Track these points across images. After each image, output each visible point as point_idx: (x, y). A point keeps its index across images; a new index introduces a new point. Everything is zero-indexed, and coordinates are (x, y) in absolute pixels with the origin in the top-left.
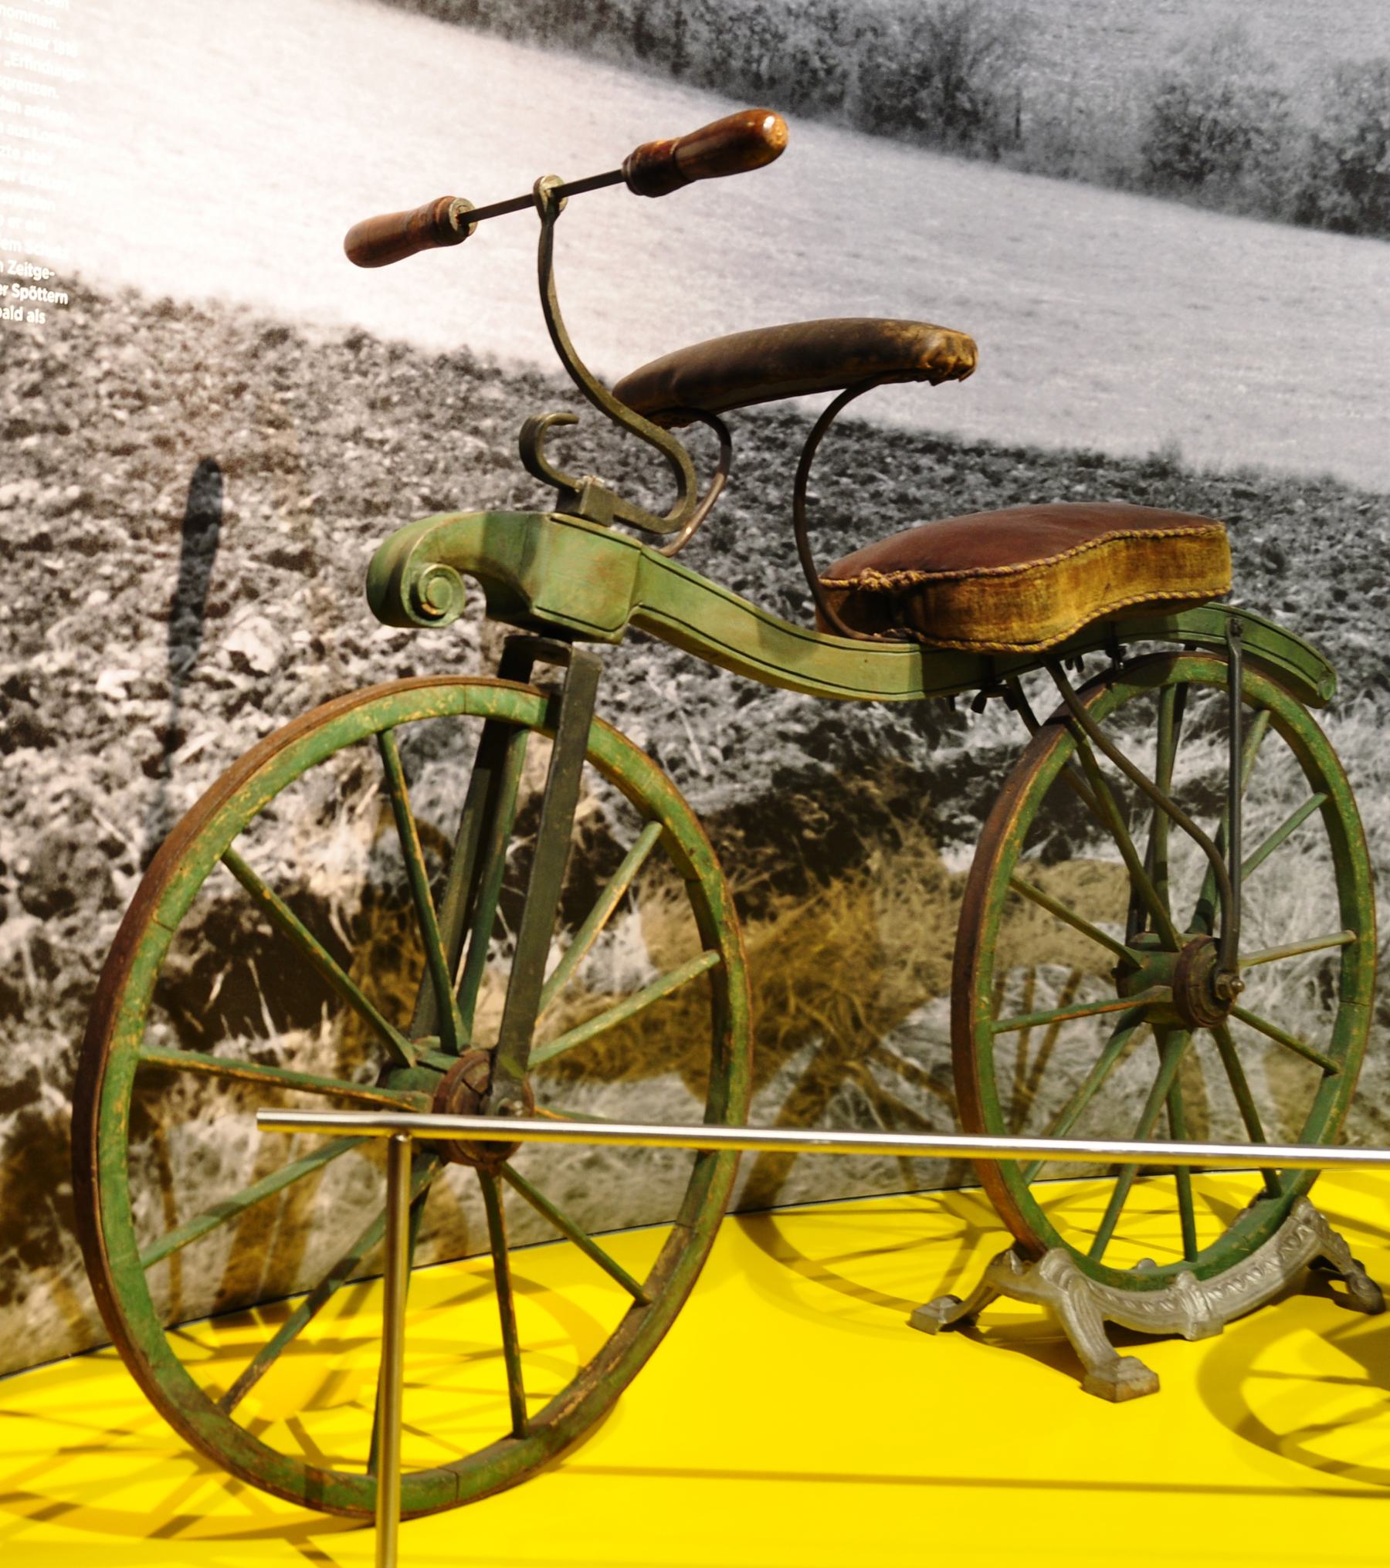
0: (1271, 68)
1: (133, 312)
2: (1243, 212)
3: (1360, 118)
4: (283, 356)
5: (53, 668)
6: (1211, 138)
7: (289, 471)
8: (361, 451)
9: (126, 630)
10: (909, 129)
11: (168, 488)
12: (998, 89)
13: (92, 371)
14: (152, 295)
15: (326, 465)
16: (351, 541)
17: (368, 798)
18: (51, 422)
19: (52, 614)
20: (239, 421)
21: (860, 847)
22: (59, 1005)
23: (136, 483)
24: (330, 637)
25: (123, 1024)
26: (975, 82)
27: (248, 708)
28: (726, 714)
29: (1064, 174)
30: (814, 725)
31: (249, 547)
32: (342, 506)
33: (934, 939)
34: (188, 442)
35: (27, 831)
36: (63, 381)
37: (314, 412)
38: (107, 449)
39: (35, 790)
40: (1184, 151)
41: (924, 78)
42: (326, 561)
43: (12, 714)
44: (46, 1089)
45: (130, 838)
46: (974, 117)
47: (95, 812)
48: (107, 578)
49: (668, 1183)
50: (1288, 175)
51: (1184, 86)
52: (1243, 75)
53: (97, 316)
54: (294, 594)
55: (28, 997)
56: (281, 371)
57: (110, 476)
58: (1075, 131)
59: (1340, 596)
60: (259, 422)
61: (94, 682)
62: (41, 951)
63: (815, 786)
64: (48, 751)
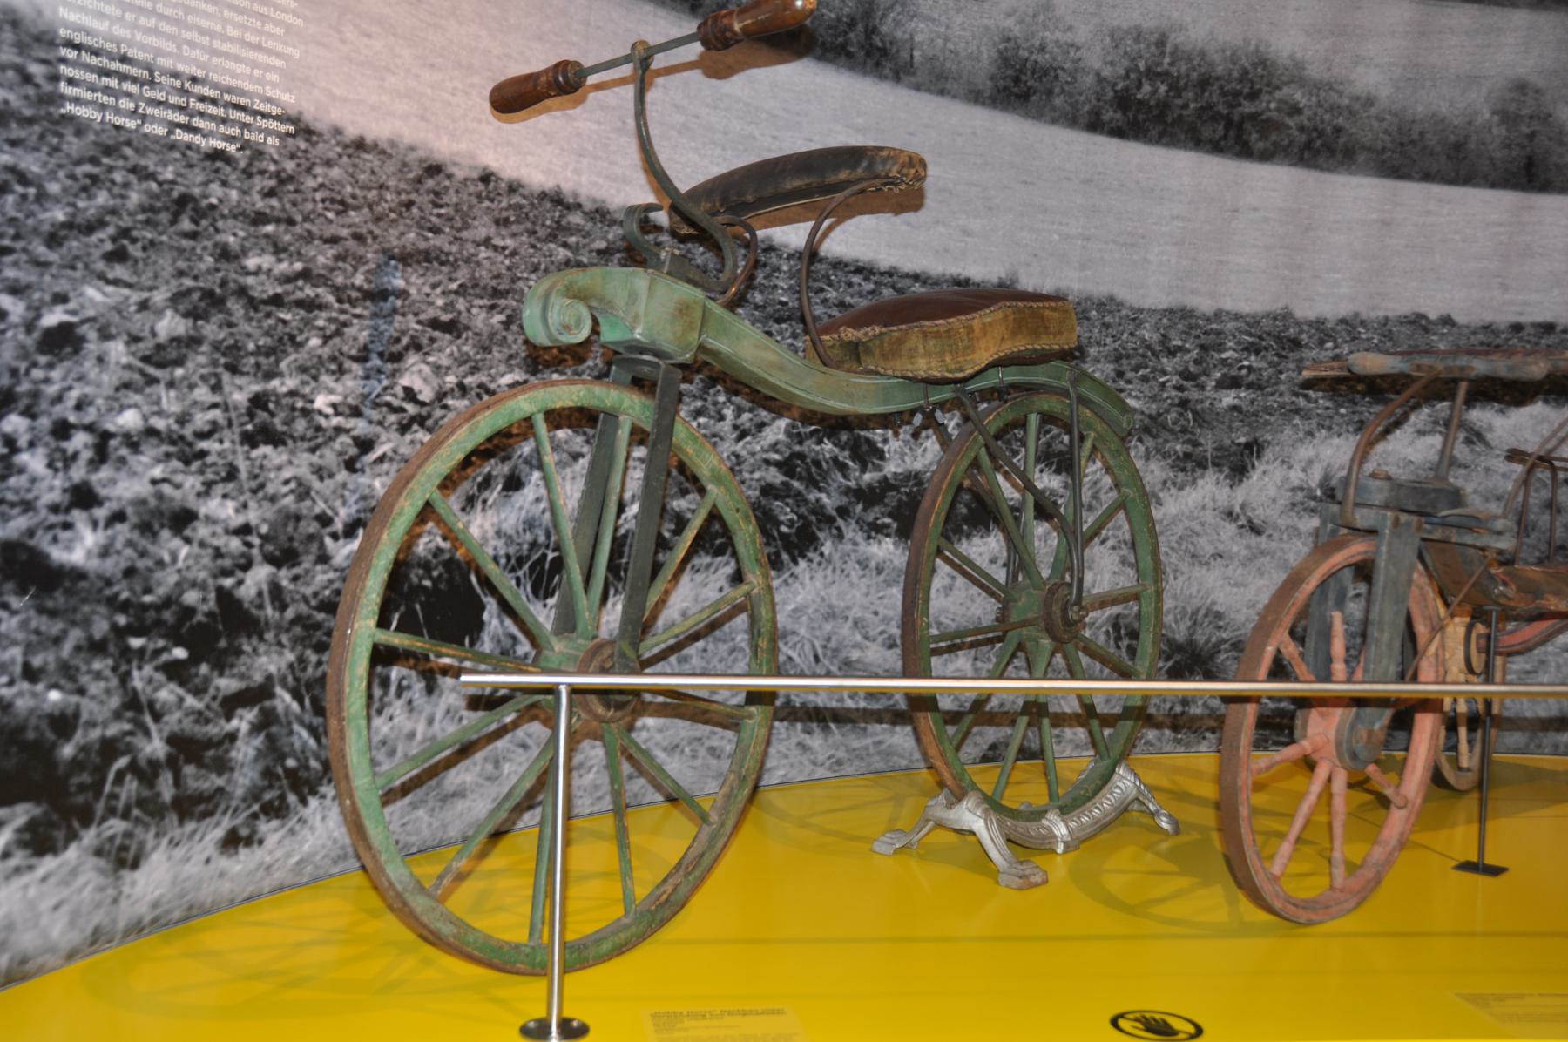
0: (1070, 28)
1: (338, 144)
2: (1054, 121)
3: (1126, 63)
4: (438, 184)
5: (284, 389)
6: (1033, 73)
7: (442, 264)
8: (490, 253)
9: (333, 367)
10: (843, 58)
11: (362, 269)
12: (899, 34)
13: (311, 183)
14: (352, 132)
15: (467, 261)
16: (484, 315)
17: (495, 494)
18: (283, 215)
19: (284, 352)
20: (409, 227)
21: (817, 539)
22: (288, 630)
23: (340, 264)
24: (468, 380)
25: (364, 612)
26: (884, 29)
27: (415, 427)
28: (728, 446)
29: (942, 92)
30: (787, 454)
31: (416, 314)
32: (478, 291)
33: (866, 601)
34: (375, 238)
35: (266, 504)
36: (291, 188)
37: (459, 224)
38: (321, 238)
39: (272, 475)
40: (1017, 80)
41: (852, 24)
42: (467, 328)
43: (257, 420)
44: (279, 690)
45: (337, 514)
46: (884, 52)
47: (313, 494)
48: (321, 329)
49: (694, 768)
50: (1082, 98)
51: (1016, 38)
52: (1053, 33)
53: (314, 144)
54: (447, 350)
55: (267, 623)
56: (437, 194)
57: (323, 258)
58: (948, 64)
59: (1120, 374)
60: (422, 228)
61: (312, 401)
62: (276, 590)
63: (788, 496)
64: (281, 448)
